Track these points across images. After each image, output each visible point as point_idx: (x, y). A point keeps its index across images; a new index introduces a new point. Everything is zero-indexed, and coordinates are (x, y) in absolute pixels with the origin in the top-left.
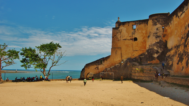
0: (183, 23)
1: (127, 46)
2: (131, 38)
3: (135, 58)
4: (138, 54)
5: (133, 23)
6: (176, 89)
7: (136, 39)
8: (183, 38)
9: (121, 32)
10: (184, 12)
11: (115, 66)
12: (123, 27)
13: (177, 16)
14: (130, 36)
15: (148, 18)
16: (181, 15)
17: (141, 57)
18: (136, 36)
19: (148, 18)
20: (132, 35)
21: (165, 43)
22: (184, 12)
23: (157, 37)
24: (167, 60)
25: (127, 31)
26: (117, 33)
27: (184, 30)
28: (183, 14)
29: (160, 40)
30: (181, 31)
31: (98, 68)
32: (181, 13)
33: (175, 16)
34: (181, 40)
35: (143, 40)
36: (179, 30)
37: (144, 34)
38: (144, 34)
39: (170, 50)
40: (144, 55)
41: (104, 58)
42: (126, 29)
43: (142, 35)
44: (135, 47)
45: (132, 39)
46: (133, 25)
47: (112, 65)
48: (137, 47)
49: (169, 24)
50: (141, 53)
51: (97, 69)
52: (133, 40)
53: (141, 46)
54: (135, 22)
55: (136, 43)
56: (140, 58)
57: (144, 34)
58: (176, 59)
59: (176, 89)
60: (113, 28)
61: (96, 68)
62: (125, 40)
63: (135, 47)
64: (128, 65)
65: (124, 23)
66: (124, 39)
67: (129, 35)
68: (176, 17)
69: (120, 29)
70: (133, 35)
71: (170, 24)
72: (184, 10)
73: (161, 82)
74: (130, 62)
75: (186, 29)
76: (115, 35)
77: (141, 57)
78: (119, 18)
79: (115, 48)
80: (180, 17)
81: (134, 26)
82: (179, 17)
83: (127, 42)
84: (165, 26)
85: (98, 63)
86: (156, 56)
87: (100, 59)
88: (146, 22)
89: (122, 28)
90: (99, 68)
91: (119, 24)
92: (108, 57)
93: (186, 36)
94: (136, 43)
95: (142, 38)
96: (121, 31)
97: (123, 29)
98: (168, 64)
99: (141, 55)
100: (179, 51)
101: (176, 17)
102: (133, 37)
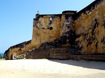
0: (90, 18)
1: (45, 33)
2: (48, 27)
3: (52, 42)
4: (53, 39)
5: (50, 16)
7: (51, 28)
8: (91, 29)
10: (92, 11)
11: (36, 49)
12: (42, 19)
13: (85, 13)
14: (47, 26)
15: (61, 13)
16: (88, 13)
17: (56, 41)
18: (52, 25)
19: (62, 13)
20: (49, 25)
22: (92, 11)
23: (69, 27)
24: (77, 44)
27: (91, 23)
28: (91, 13)
29: (71, 30)
30: (89, 23)
31: (21, 50)
32: (89, 11)
33: (83, 13)
34: (89, 30)
35: (57, 29)
36: (87, 23)
37: (58, 25)
38: (58, 25)
39: (79, 36)
40: (58, 40)
41: (26, 42)
42: (44, 20)
44: (51, 34)
45: (48, 28)
46: (49, 18)
47: (33, 47)
48: (52, 34)
49: (77, 19)
50: (55, 38)
53: (55, 33)
55: (52, 31)
60: (34, 19)
61: (19, 51)
62: (44, 28)
63: (51, 34)
64: (47, 47)
65: (42, 16)
66: (42, 27)
67: (47, 25)
68: (84, 14)
70: (50, 25)
72: (92, 10)
73: (96, 57)
74: (48, 45)
75: (93, 22)
78: (38, 12)
79: (36, 34)
80: (87, 14)
81: (50, 18)
82: (86, 14)
83: (45, 31)
85: (21, 46)
86: (68, 40)
87: (23, 43)
90: (22, 50)
91: (39, 17)
92: (29, 42)
93: (93, 27)
94: (52, 31)
95: (56, 27)
98: (78, 47)
99: (56, 40)
100: (87, 37)
101: (84, 14)
102: (50, 27)
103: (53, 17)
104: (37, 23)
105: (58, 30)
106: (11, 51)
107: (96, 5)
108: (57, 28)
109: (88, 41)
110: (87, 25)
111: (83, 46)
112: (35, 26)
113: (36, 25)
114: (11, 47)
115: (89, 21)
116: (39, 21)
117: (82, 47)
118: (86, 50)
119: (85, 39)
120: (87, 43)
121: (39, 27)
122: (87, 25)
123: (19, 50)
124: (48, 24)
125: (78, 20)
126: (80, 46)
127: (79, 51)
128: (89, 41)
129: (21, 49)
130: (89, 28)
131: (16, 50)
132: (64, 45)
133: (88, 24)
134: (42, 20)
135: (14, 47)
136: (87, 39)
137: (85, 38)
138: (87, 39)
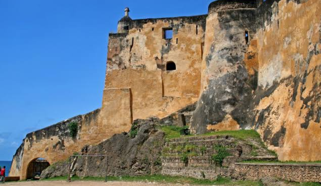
6: (292, 106)
9: (131, 47)
18: (170, 57)
20: (162, 54)
21: (252, 76)
24: (262, 118)
25: (149, 43)
26: (122, 48)
31: (61, 144)
36: (299, 35)
43: (190, 55)
51: (61, 148)
52: (165, 68)
54: (171, 21)
56: (183, 116)
57: (193, 53)
58: (281, 94)
59: (292, 106)
61: (58, 146)
67: (155, 56)
69: (129, 37)
70: (165, 55)
71: (265, 24)
76: (117, 53)
77: (185, 114)
84: (250, 32)
85: (64, 130)
88: (200, 23)
89: (134, 34)
96: (131, 44)
97: (138, 38)
98: (267, 132)
100: (303, 90)
103: (178, 25)
104: (121, 50)
105: (194, 74)
106: (29, 149)
107: (230, 5)
108: (190, 67)
109: (309, 103)
110: (301, 40)
111: (287, 128)
112: (114, 60)
113: (116, 55)
114: (29, 136)
115: (308, 22)
116: (127, 41)
117: (283, 131)
118: (300, 143)
119: (294, 99)
120: (305, 112)
121: (127, 64)
122: (301, 40)
123: (55, 147)
124: (86, 144)
125: (268, 28)
126: (276, 129)
127: (271, 148)
128: (312, 106)
129: (63, 141)
130: (311, 52)
131: (46, 144)
132: (212, 124)
133: (305, 37)
134: (138, 38)
135: (38, 134)
136: (302, 98)
137: (295, 94)
138: (302, 98)
